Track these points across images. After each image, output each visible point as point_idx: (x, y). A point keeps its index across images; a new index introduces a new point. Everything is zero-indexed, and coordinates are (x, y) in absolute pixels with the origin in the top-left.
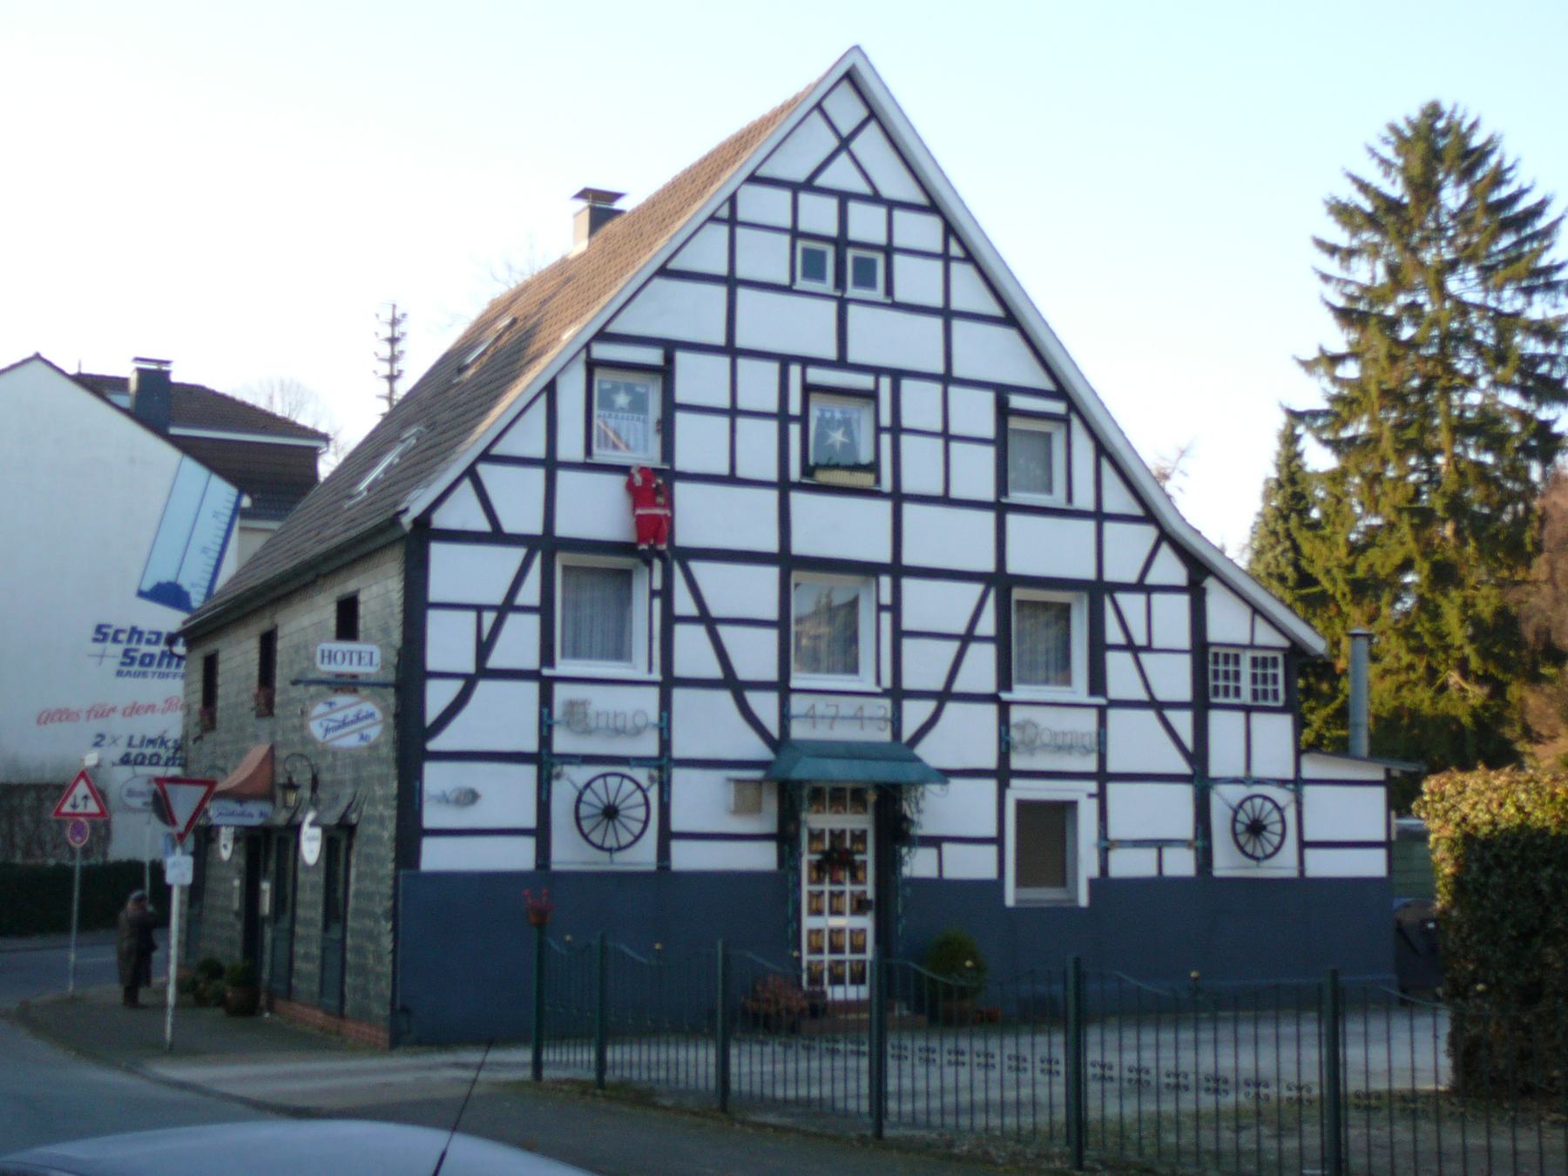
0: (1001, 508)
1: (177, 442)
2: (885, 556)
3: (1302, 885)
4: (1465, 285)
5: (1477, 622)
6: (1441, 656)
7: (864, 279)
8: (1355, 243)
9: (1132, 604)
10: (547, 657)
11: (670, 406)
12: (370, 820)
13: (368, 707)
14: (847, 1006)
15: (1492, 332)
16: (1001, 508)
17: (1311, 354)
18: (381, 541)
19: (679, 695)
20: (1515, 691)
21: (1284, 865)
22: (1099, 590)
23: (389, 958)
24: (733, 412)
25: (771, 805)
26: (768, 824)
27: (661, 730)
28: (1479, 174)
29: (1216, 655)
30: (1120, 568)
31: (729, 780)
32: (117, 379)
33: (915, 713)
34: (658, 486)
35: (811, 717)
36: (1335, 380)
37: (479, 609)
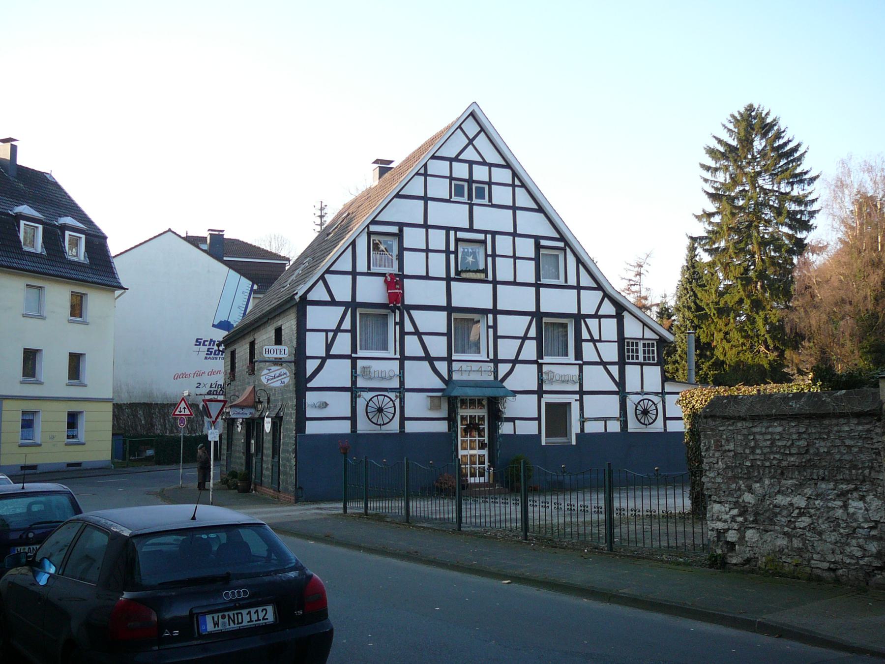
0: (538, 286)
1: (226, 263)
2: (490, 306)
3: (666, 433)
4: (765, 182)
5: (771, 324)
6: (756, 339)
7: (481, 195)
8: (718, 165)
9: (593, 323)
10: (354, 349)
11: (402, 249)
12: (287, 415)
13: (284, 370)
14: (479, 485)
15: (777, 202)
16: (538, 286)
17: (700, 213)
18: (288, 306)
19: (407, 363)
20: (788, 354)
21: (658, 427)
22: (579, 318)
23: (294, 468)
24: (427, 251)
25: (445, 406)
26: (444, 414)
27: (400, 377)
28: (770, 135)
29: (628, 343)
30: (588, 308)
31: (428, 396)
32: (203, 237)
33: (503, 369)
34: (397, 280)
35: (460, 371)
36: (710, 223)
37: (327, 331)
